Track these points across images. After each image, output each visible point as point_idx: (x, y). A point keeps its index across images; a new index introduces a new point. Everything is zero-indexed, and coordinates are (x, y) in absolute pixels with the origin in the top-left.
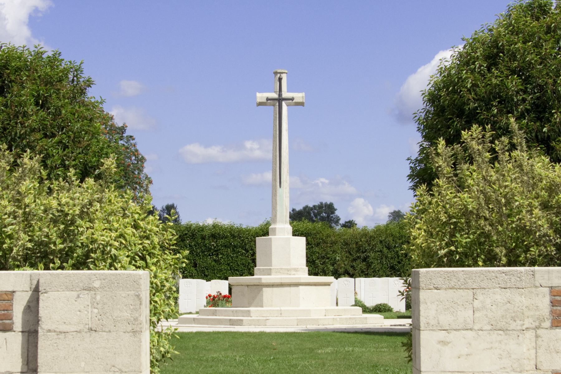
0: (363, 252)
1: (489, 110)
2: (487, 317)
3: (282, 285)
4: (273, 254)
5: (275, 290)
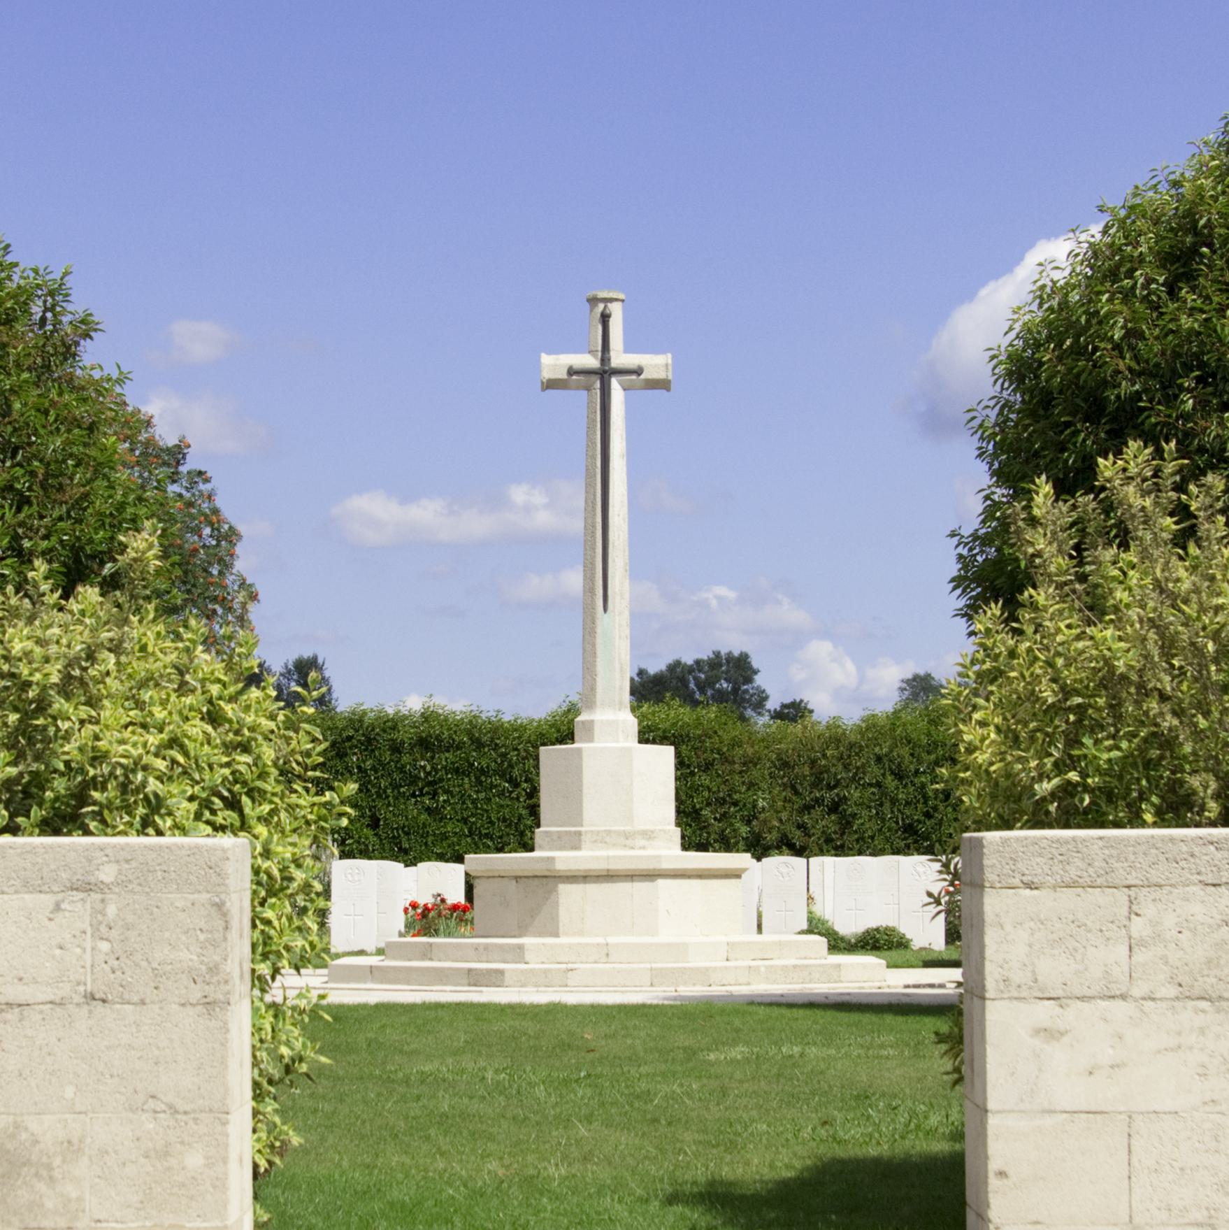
1: (1171, 399)
2: (1166, 963)
3: (609, 876)
4: (585, 790)
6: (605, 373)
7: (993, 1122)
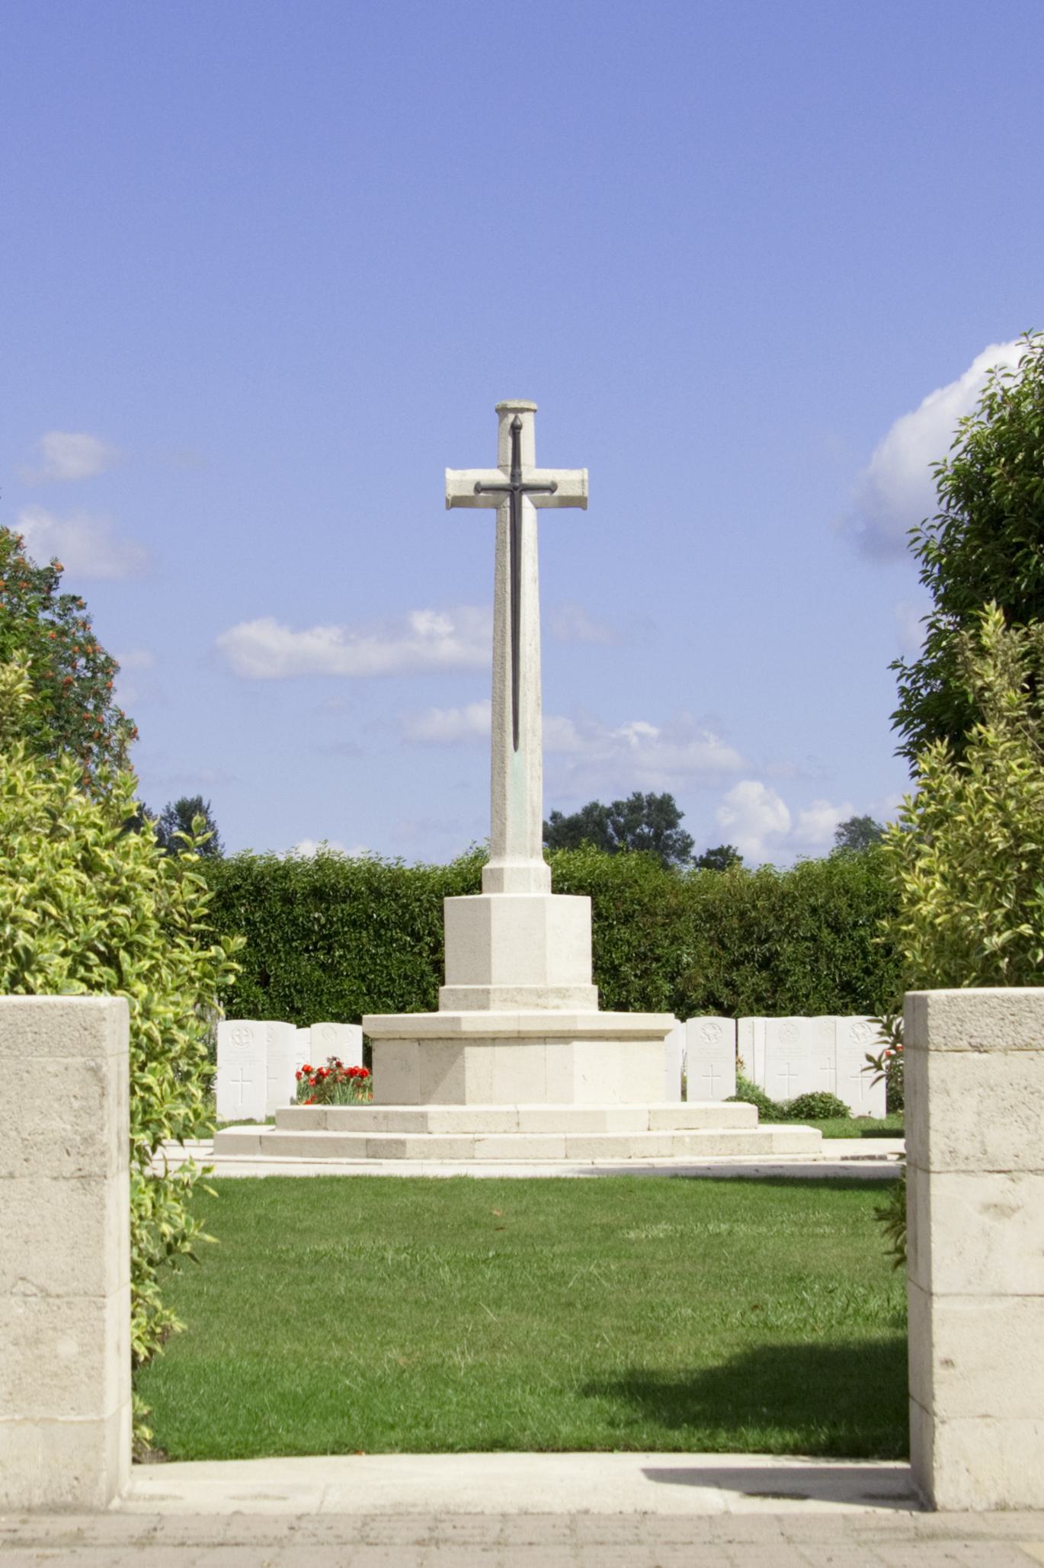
0: (761, 942)
5: (502, 1052)
6: (515, 490)
7: (938, 1306)
